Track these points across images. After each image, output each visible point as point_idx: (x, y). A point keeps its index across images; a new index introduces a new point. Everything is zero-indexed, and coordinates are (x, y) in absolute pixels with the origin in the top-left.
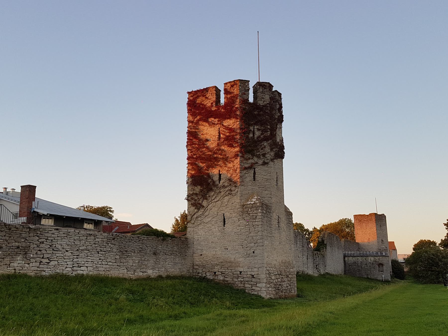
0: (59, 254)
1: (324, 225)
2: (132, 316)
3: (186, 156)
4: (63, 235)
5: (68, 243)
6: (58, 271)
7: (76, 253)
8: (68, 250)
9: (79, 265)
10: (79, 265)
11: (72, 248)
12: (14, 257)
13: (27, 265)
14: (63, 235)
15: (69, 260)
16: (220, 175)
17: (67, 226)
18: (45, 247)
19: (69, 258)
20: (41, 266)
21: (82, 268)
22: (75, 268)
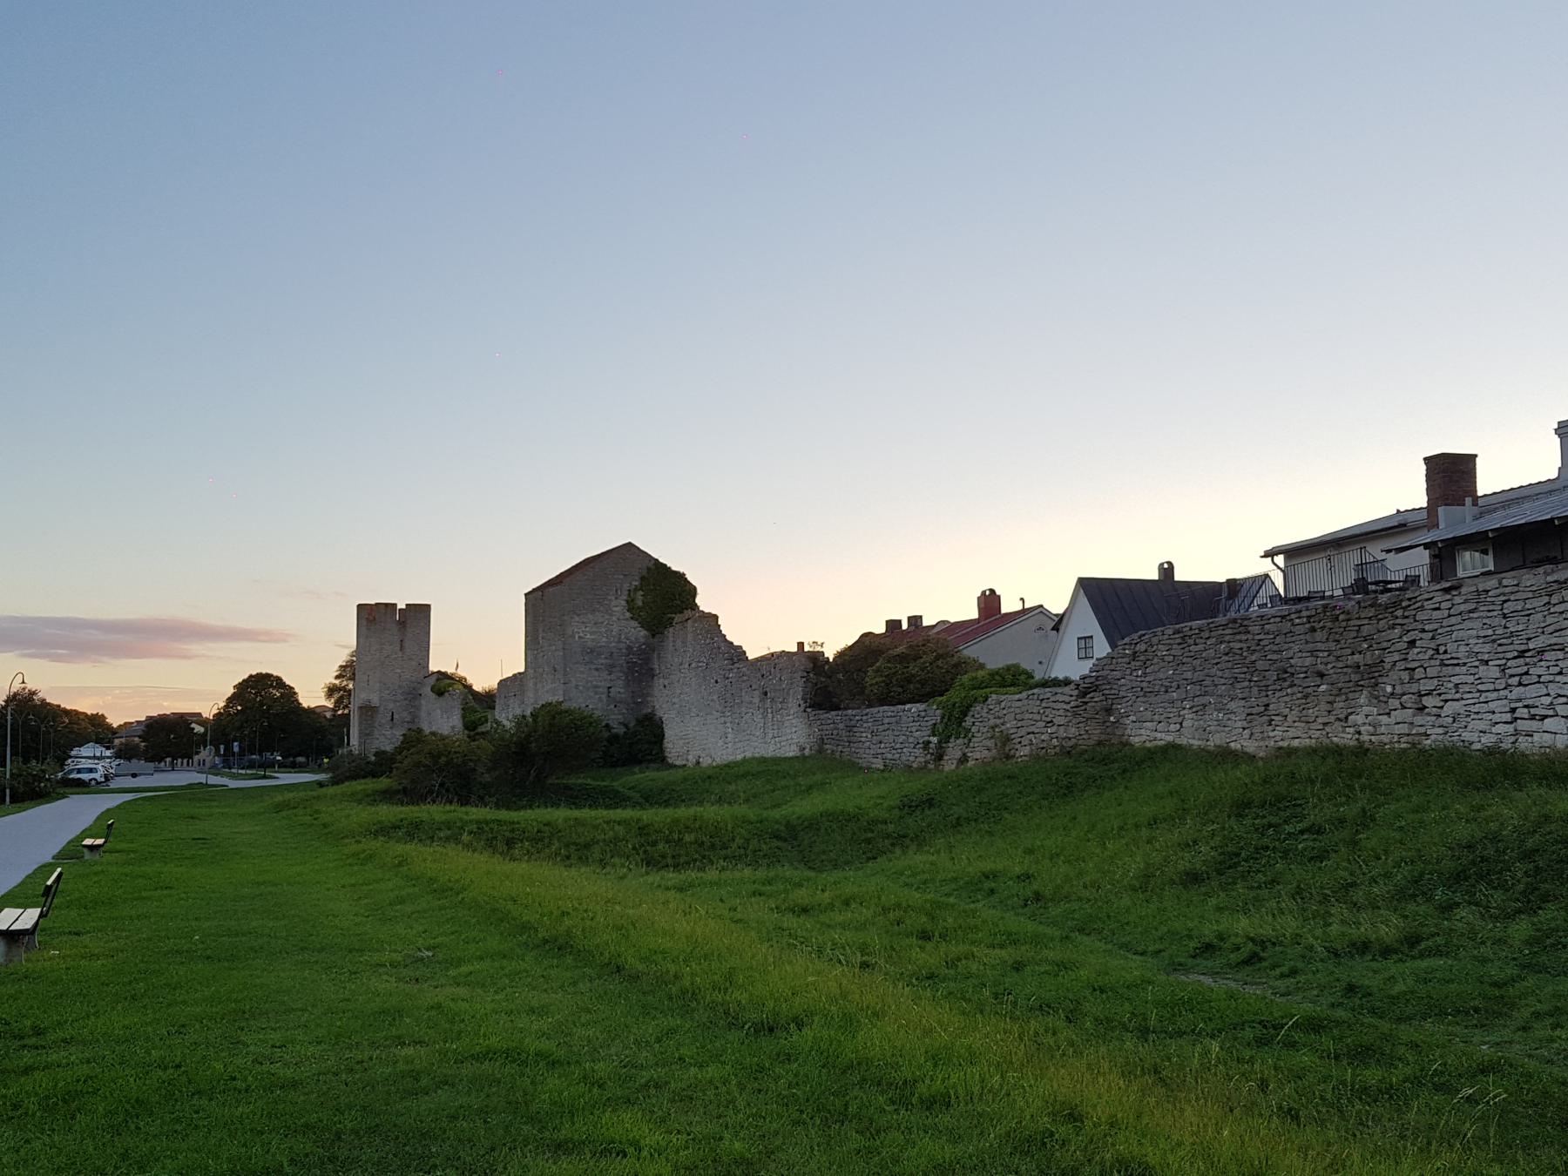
0: (1462, 676)
1: (915, 621)
2: (397, 957)
3: (342, 657)
4: (1462, 607)
5: (1482, 633)
6: (1466, 736)
7: (1517, 667)
8: (1486, 657)
9: (1533, 711)
10: (1533, 711)
11: (1500, 649)
12: (1351, 696)
13: (1384, 719)
14: (1462, 607)
15: (1495, 695)
16: (402, 648)
17: (1539, 563)
18: (1421, 656)
19: (1491, 687)
20: (1419, 720)
21: (1549, 724)
22: (1523, 725)
